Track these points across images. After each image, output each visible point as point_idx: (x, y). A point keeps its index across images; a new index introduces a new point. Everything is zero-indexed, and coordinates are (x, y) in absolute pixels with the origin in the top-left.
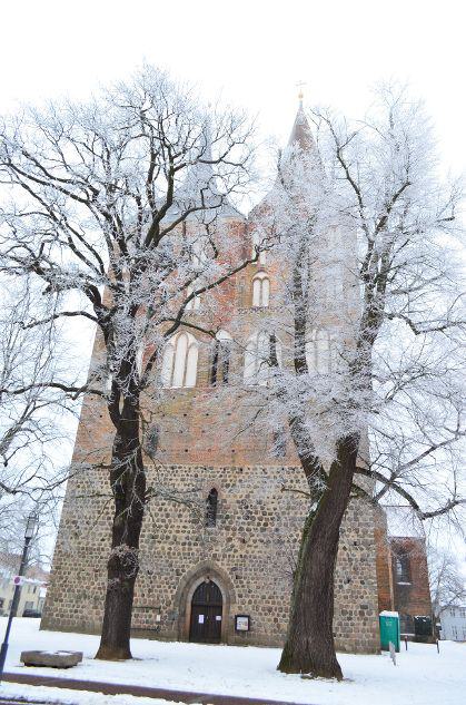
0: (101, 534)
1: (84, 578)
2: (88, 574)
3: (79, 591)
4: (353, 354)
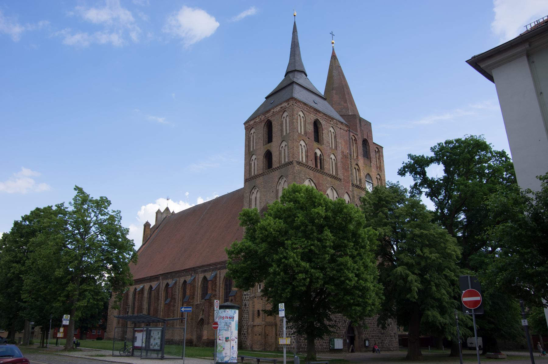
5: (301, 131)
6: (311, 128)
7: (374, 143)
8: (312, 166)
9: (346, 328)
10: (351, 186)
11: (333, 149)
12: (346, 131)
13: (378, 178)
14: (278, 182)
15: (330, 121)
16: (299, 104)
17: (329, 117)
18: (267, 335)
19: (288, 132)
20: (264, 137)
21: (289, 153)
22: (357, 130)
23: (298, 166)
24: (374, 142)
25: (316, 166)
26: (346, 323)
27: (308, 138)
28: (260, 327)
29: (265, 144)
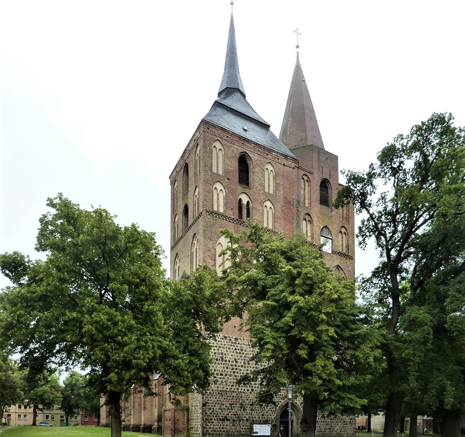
0: (230, 382)
1: (224, 409)
2: (226, 407)
3: (223, 417)
4: (57, 411)
6: (234, 165)
7: (339, 184)
8: (233, 217)
9: (277, 413)
14: (192, 243)
15: (267, 154)
16: (214, 130)
17: (264, 148)
18: (178, 420)
20: (183, 189)
23: (209, 217)
24: (339, 183)
26: (277, 408)
28: (170, 412)
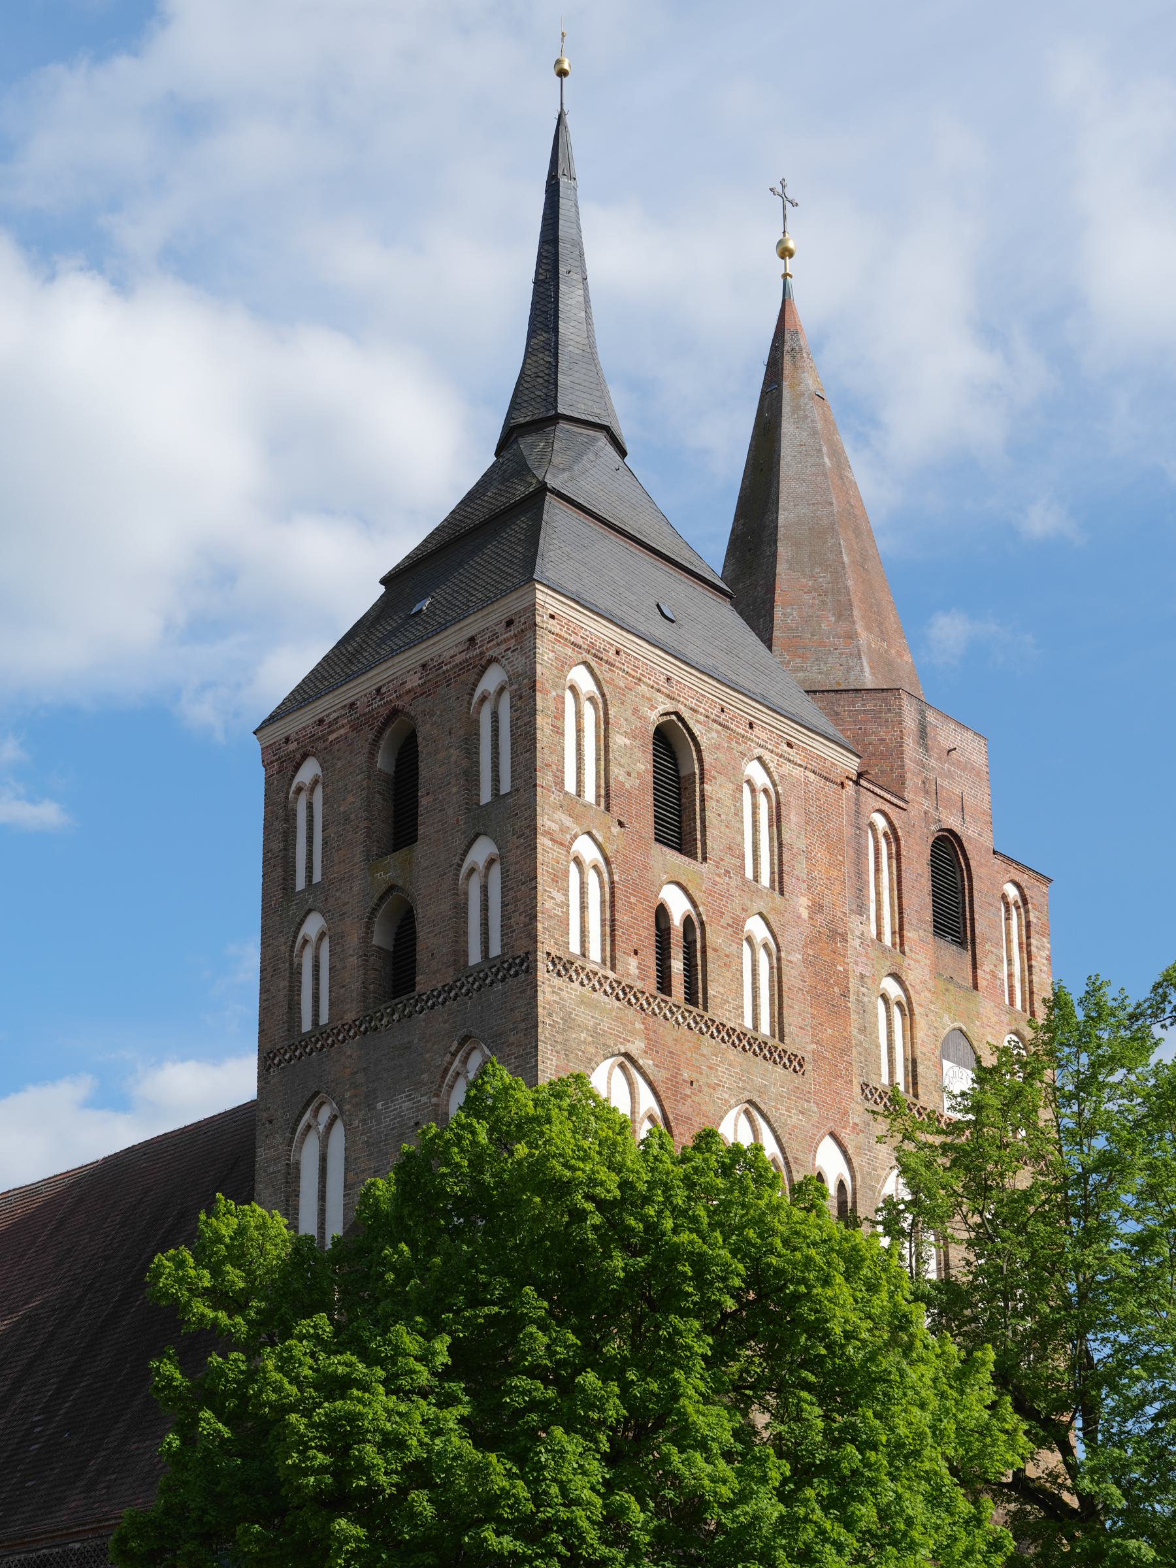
5: (579, 783)
10: (859, 1098)
11: (884, 948)
12: (842, 785)
13: (1011, 899)
19: (505, 787)
21: (511, 908)
22: (902, 779)
25: (664, 985)
27: (621, 824)
29: (375, 850)
